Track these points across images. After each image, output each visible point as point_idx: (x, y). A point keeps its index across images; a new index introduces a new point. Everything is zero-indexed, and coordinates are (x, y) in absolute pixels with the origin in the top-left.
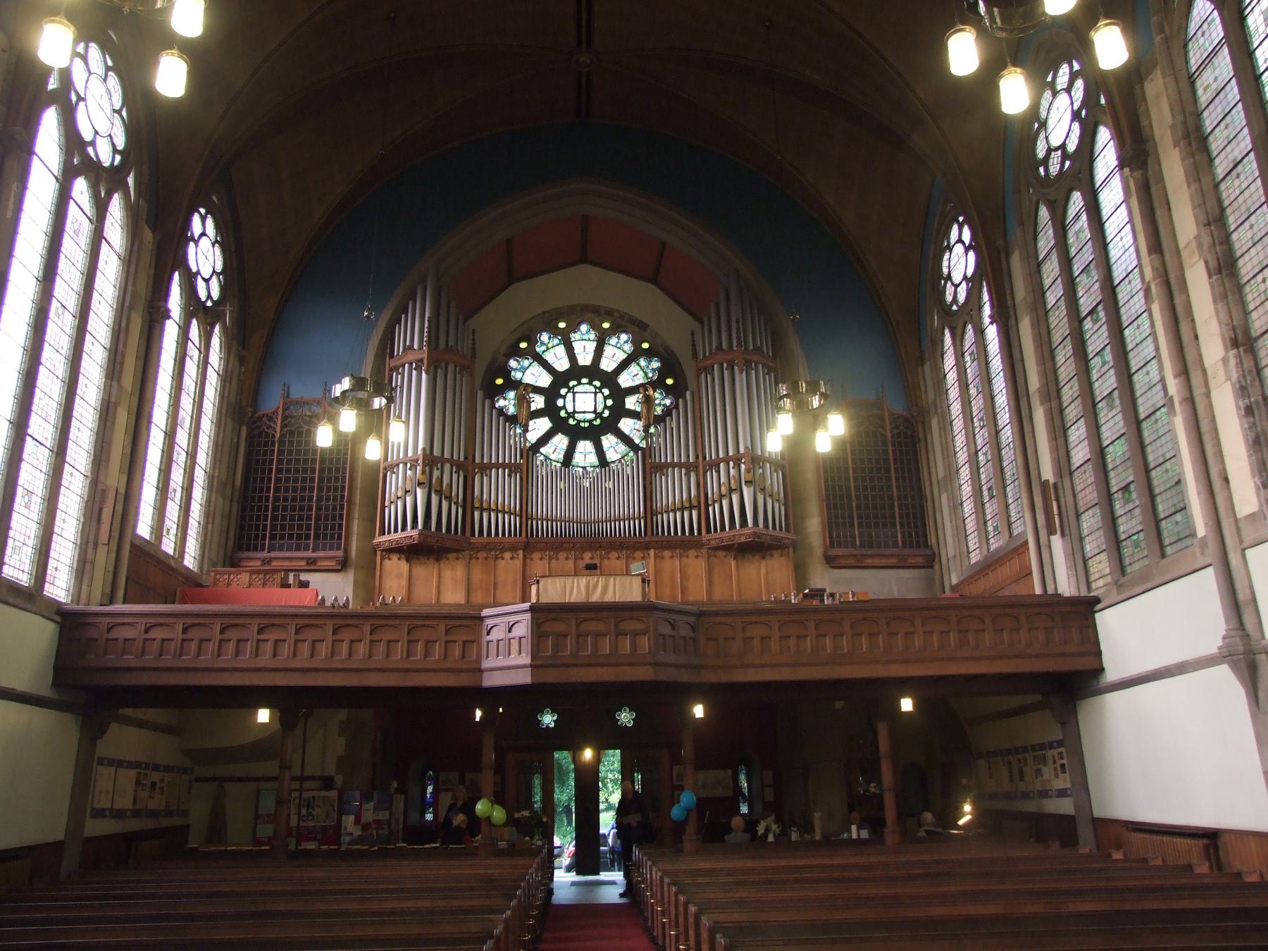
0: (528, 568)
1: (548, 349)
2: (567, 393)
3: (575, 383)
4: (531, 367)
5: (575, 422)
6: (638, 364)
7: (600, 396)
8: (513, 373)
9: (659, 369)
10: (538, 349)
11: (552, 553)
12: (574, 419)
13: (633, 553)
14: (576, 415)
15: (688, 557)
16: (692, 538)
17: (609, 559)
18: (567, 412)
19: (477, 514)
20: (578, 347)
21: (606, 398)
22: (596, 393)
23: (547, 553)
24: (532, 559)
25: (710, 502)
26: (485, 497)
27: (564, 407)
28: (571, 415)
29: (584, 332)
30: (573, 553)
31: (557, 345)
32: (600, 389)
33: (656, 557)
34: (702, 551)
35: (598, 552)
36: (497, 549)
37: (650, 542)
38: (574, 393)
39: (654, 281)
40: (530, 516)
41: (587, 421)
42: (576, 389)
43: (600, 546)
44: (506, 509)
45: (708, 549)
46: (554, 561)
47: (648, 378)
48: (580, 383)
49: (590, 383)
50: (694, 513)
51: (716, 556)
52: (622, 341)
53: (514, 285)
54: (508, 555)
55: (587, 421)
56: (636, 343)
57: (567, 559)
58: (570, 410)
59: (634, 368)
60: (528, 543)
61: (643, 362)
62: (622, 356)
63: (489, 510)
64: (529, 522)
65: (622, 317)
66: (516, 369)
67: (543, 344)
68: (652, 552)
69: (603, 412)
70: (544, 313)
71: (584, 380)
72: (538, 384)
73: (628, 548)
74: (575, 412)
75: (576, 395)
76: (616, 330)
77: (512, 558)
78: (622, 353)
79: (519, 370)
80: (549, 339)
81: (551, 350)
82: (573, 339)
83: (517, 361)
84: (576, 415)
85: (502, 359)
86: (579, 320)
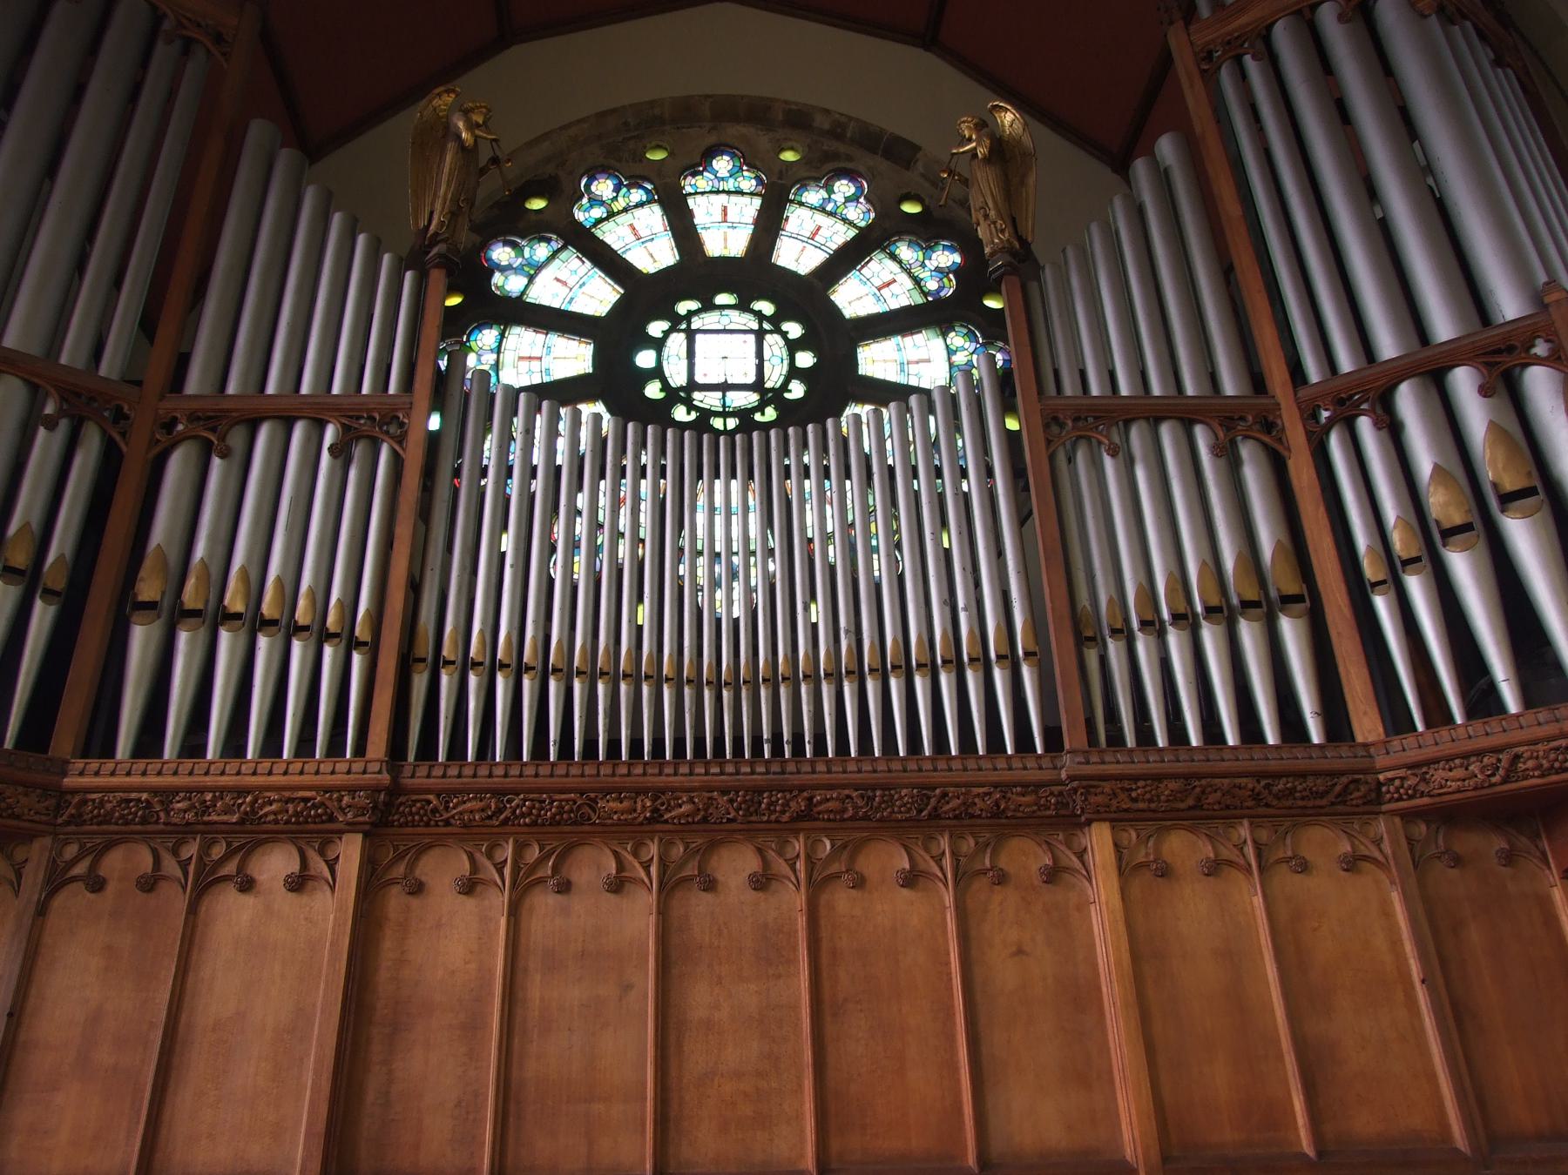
0: (388, 944)
1: (611, 215)
2: (667, 334)
3: (693, 305)
4: (557, 262)
5: (693, 415)
6: (894, 257)
7: (773, 343)
8: (498, 279)
9: (958, 271)
10: (580, 216)
11: (968, 845)
12: (691, 407)
13: (856, 848)
14: (697, 395)
15: (1304, 867)
16: (1297, 759)
17: (860, 883)
18: (666, 386)
19: (141, 639)
20: (704, 210)
21: (793, 347)
22: (760, 335)
23: (507, 851)
24: (417, 889)
25: (1371, 570)
26: (200, 550)
27: (658, 373)
28: (681, 395)
29: (723, 173)
30: (944, 843)
31: (640, 205)
32: (776, 320)
33: (1126, 869)
34: (1381, 826)
35: (798, 845)
36: (210, 833)
37: (1088, 783)
38: (691, 335)
39: (929, 38)
40: (425, 648)
41: (733, 414)
42: (696, 323)
43: (807, 815)
44: (302, 614)
45: (1408, 816)
46: (544, 902)
47: (925, 294)
48: (709, 306)
49: (743, 306)
50: (1291, 631)
51: (1457, 861)
52: (839, 197)
53: (516, 51)
54: (276, 864)
55: (733, 414)
56: (884, 206)
57: (618, 885)
58: (677, 376)
59: (879, 267)
60: (395, 790)
61: (905, 252)
62: (838, 235)
63: (257, 623)
64: (420, 683)
65: (837, 132)
66: (509, 268)
67: (596, 201)
68: (1099, 840)
69: (785, 387)
70: (602, 115)
71: (723, 299)
72: (577, 308)
73: (963, 820)
74: (692, 386)
75: (699, 337)
76: (822, 169)
77: (298, 883)
78: (841, 227)
79: (518, 270)
80: (617, 189)
81: (621, 219)
82: (688, 189)
83: (514, 245)
84: (697, 395)
85: (465, 237)
86: (711, 139)
